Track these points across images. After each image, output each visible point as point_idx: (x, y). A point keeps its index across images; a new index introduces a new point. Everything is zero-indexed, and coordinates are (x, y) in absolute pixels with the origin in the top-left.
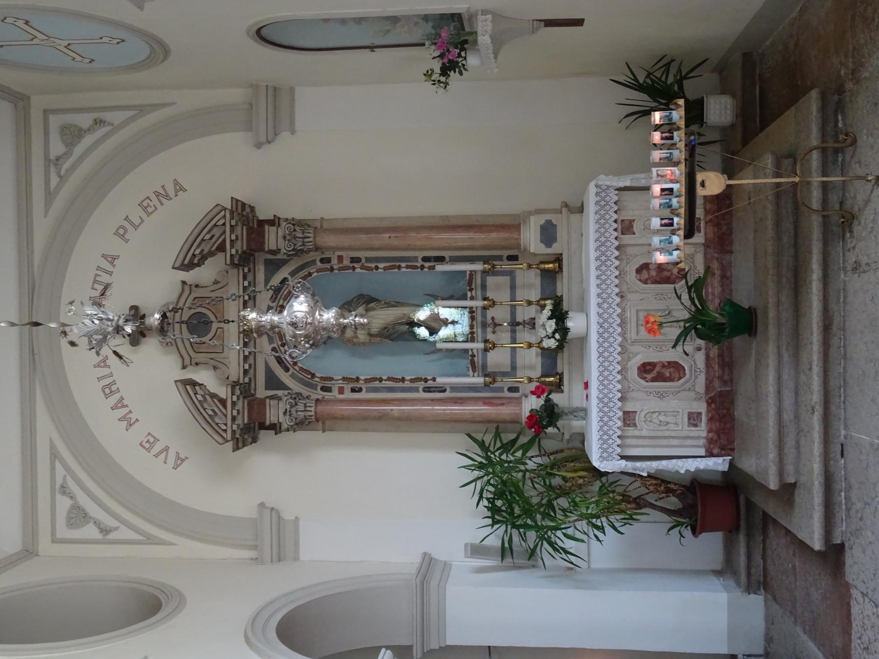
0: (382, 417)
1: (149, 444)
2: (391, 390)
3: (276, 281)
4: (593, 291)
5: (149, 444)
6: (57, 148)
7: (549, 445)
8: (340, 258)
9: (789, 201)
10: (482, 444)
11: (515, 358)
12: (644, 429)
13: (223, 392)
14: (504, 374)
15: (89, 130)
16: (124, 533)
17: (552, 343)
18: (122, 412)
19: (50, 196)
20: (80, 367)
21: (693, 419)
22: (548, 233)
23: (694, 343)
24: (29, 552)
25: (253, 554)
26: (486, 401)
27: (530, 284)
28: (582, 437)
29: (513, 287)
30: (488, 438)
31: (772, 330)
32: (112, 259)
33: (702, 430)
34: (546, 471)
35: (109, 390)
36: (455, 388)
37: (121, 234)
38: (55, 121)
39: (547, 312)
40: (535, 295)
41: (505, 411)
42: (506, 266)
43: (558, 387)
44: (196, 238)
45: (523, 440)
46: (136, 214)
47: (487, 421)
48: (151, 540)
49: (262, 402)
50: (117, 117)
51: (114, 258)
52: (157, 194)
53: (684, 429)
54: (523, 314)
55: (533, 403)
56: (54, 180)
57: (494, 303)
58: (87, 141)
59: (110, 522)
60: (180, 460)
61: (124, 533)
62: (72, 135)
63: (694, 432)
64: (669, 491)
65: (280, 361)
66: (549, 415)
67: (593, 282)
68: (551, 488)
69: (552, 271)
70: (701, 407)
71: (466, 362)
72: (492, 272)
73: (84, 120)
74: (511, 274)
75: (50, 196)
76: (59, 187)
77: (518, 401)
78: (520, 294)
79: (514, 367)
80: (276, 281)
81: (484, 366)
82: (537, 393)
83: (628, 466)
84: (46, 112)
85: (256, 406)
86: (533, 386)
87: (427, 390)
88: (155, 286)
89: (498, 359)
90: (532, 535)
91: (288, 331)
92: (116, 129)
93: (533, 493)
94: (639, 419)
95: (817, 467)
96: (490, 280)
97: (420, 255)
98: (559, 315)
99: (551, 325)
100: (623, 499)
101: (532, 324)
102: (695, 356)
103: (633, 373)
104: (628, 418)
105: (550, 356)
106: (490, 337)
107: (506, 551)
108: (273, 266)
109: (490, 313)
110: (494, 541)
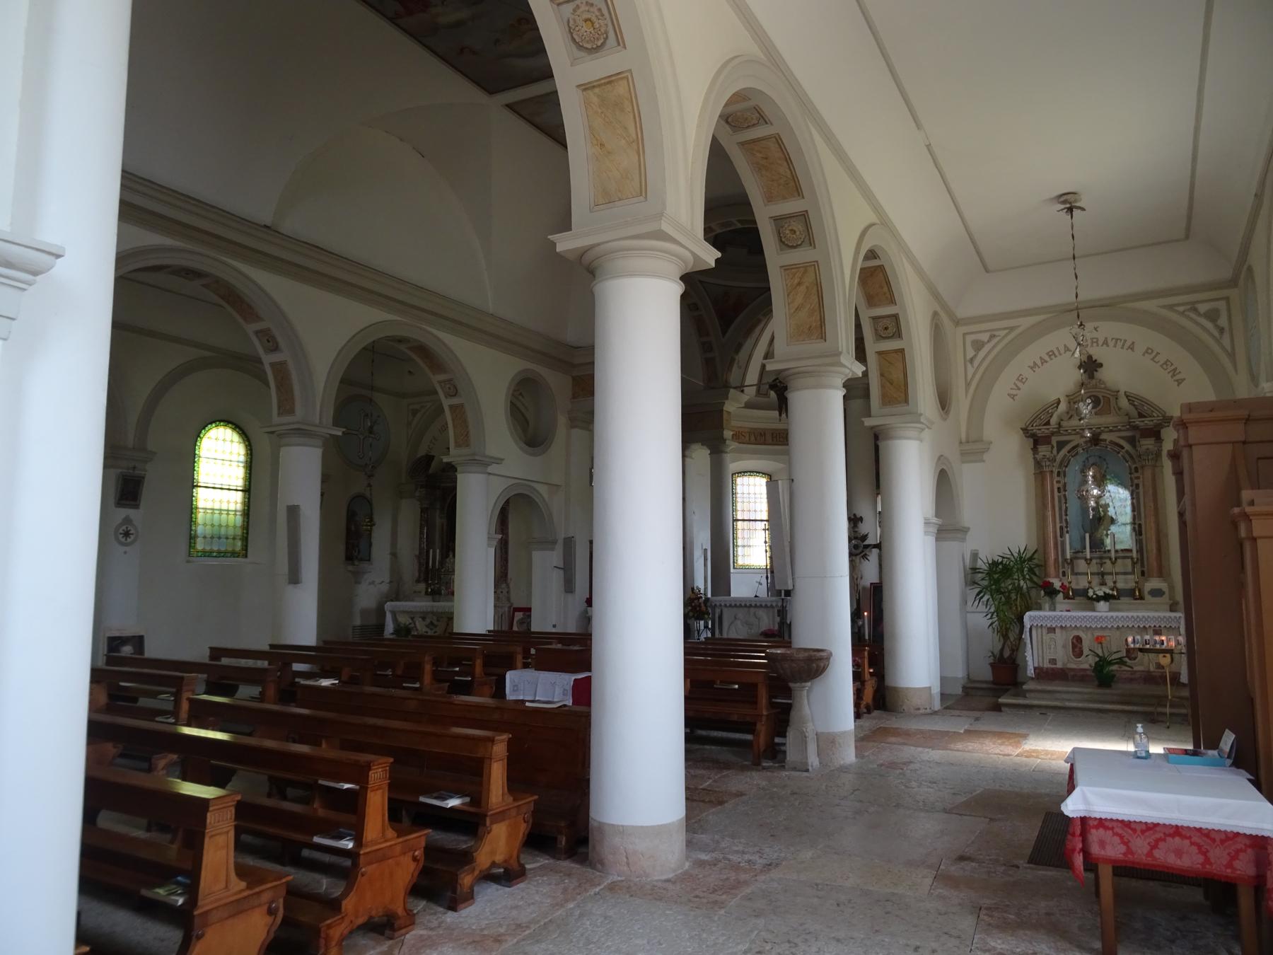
0: (1044, 506)
1: (1021, 379)
2: (1060, 509)
3: (1123, 443)
4: (1120, 614)
5: (1021, 379)
6: (1203, 308)
7: (1033, 593)
8: (1138, 478)
9: (1161, 700)
10: (1031, 559)
11: (1177, 481)
12: (1047, 637)
13: (1054, 421)
14: (1072, 570)
15: (1217, 326)
16: (971, 370)
17: (1091, 593)
18: (1039, 363)
19: (1171, 307)
20: (1063, 337)
21: (1053, 661)
22: (1157, 593)
23: (1092, 660)
24: (957, 322)
25: (964, 440)
26: (1056, 560)
27: (1125, 583)
28: (1040, 608)
29: (1125, 574)
30: (1035, 561)
31: (1100, 691)
32: (1132, 348)
33: (1047, 665)
34: (1018, 589)
35: (1051, 354)
36: (1063, 543)
37: (1148, 351)
38: (1222, 305)
39: (1108, 591)
40: (1120, 585)
41: (1052, 570)
42: (1138, 569)
43: (1067, 597)
44: (1144, 401)
45: (1035, 579)
46: (1161, 359)
47: (1046, 560)
48: (968, 385)
49: (1049, 443)
50: (1226, 341)
51: (1132, 349)
52: (1175, 370)
53: (1048, 656)
54: (1109, 580)
55: (1057, 584)
56: (1181, 309)
57: (1113, 563)
58: (1209, 325)
59: (976, 363)
60: (1013, 397)
61: (971, 370)
62: (1212, 316)
63: (1046, 661)
64: (1013, 650)
65: (1074, 448)
66: (1051, 592)
67: (1125, 614)
68: (1010, 592)
69: (1135, 595)
70: (1059, 665)
71: (1078, 547)
72: (1134, 564)
73: (1223, 321)
74: (1133, 573)
75: (1171, 307)
76: (1177, 311)
77: (1057, 576)
78: (1120, 578)
79: (1077, 574)
80: (1123, 443)
81: (1077, 558)
82: (1063, 586)
83: (1027, 629)
84: (1227, 299)
85: (1046, 440)
86: (1066, 584)
87: (1061, 528)
88: (1116, 373)
89: (1081, 565)
90: (985, 583)
91: (1084, 488)
92: (1218, 341)
93: (1007, 584)
94: (1052, 635)
95: (1036, 702)
96: (1129, 561)
97: (1142, 522)
98: (1107, 597)
99: (1101, 593)
100: (1010, 626)
101: (1103, 584)
102: (1087, 662)
103: (1076, 633)
104: (1052, 630)
105: (1083, 593)
106: (1094, 561)
107: (974, 570)
108: (1132, 441)
109: (1108, 561)
110: (980, 564)
